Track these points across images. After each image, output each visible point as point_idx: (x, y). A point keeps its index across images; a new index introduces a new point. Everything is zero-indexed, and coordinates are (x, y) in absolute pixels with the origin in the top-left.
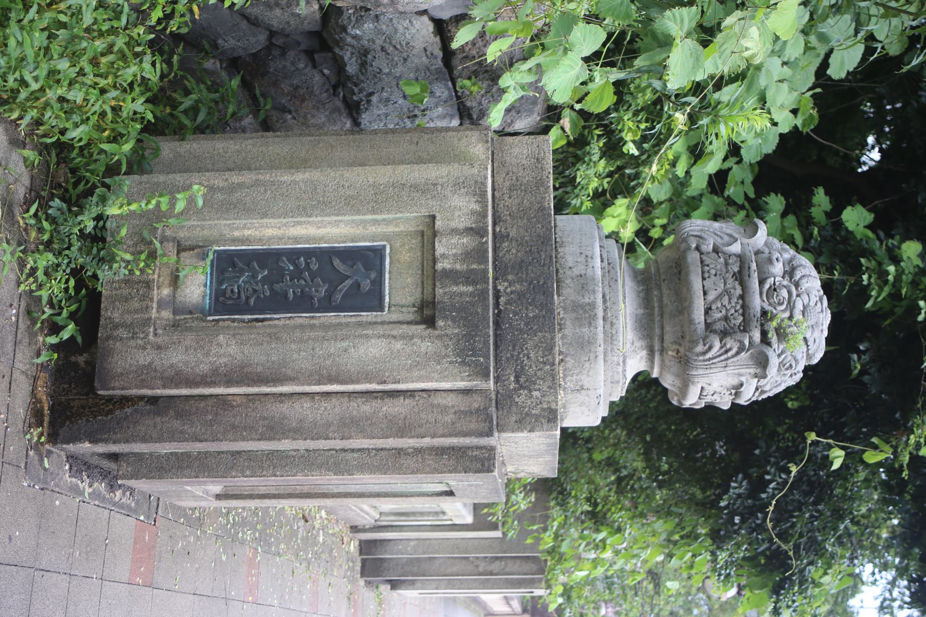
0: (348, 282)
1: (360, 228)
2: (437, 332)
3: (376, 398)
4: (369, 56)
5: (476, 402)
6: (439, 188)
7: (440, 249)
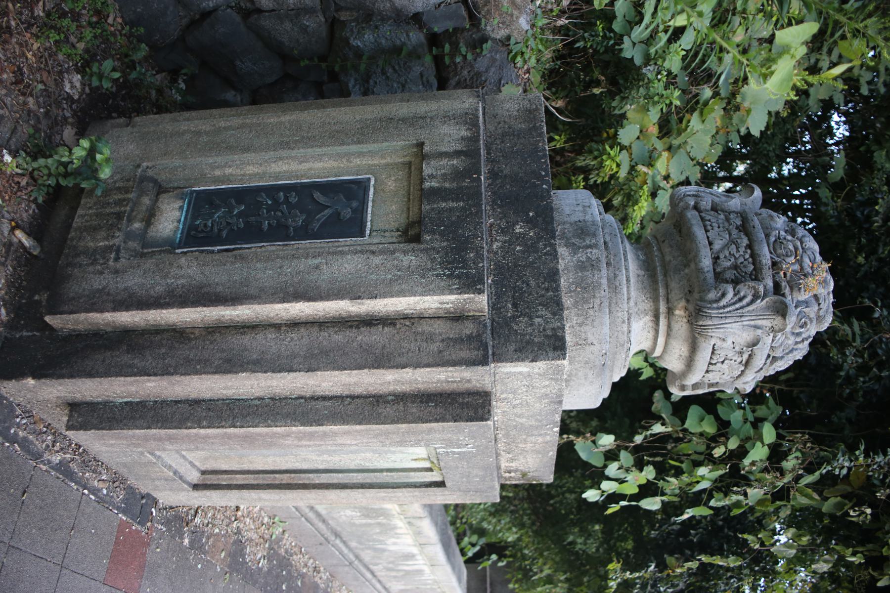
0: (327, 212)
1: (344, 160)
2: (422, 246)
3: (351, 327)
4: (371, 82)
5: (469, 328)
6: (428, 120)
7: (427, 170)
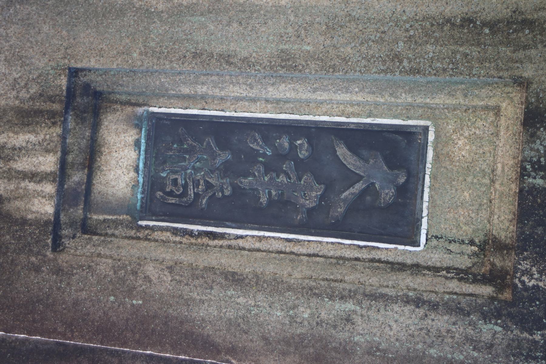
0: (358, 187)
